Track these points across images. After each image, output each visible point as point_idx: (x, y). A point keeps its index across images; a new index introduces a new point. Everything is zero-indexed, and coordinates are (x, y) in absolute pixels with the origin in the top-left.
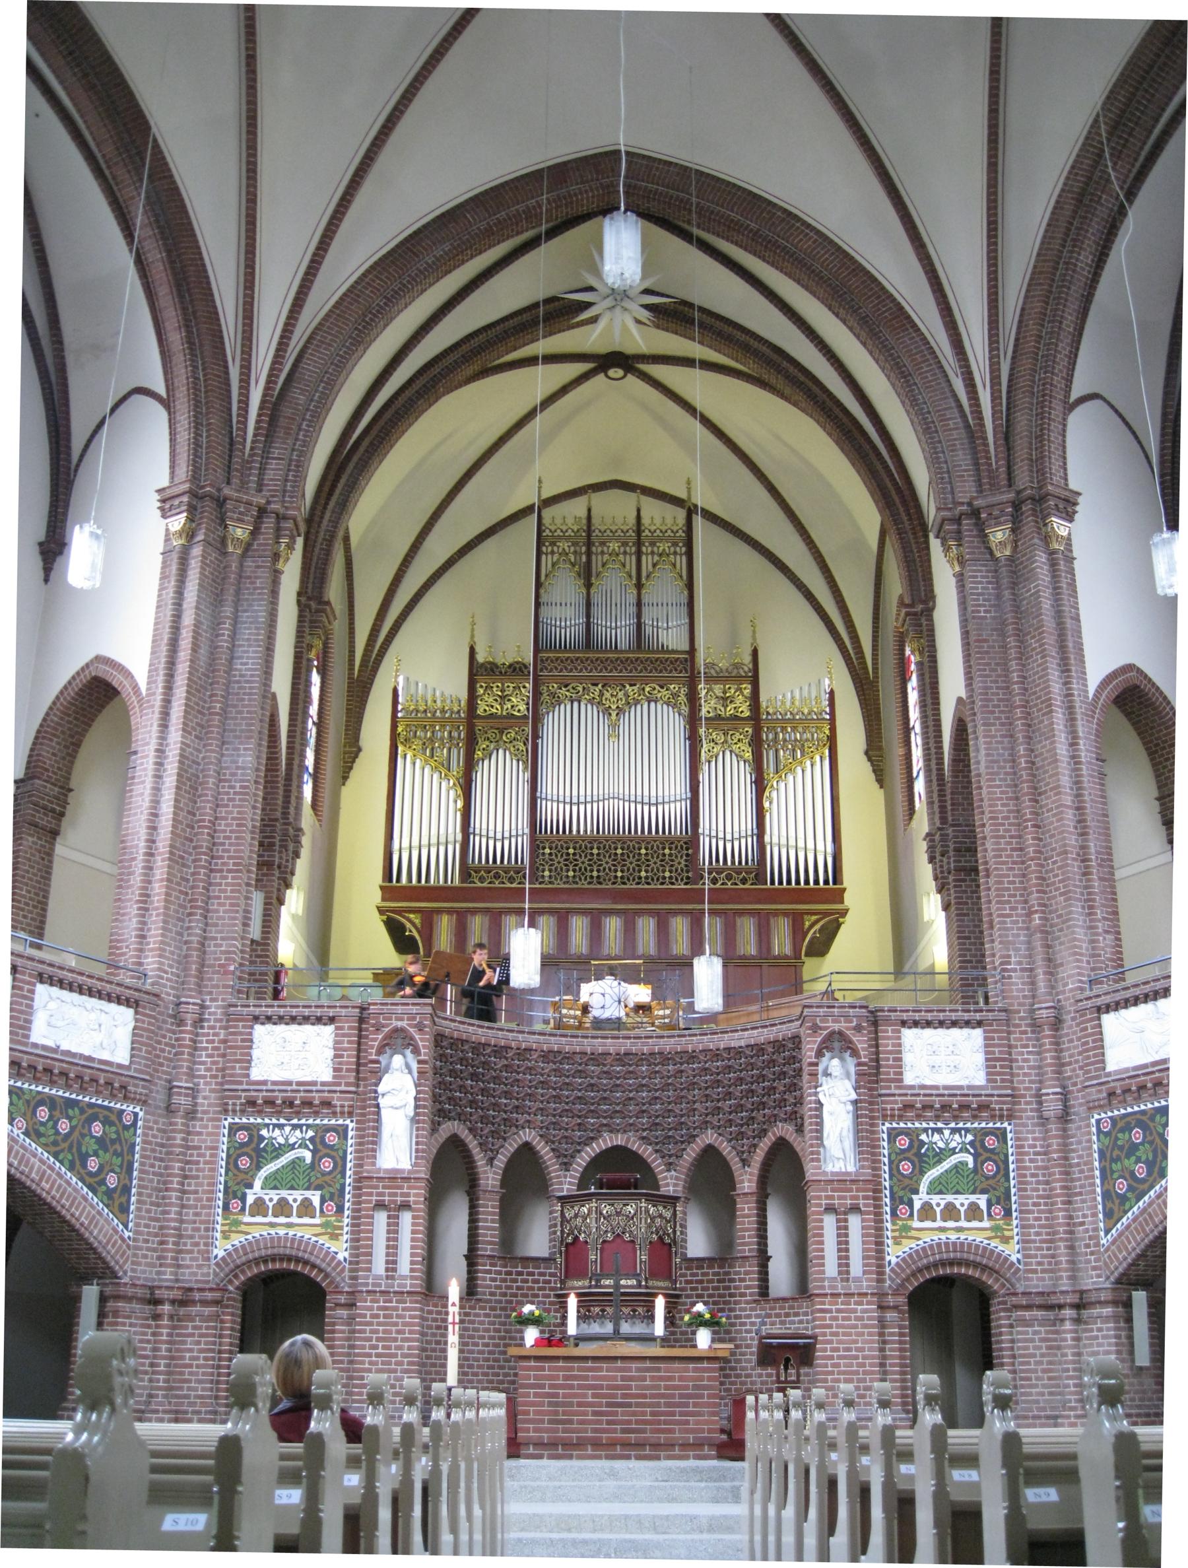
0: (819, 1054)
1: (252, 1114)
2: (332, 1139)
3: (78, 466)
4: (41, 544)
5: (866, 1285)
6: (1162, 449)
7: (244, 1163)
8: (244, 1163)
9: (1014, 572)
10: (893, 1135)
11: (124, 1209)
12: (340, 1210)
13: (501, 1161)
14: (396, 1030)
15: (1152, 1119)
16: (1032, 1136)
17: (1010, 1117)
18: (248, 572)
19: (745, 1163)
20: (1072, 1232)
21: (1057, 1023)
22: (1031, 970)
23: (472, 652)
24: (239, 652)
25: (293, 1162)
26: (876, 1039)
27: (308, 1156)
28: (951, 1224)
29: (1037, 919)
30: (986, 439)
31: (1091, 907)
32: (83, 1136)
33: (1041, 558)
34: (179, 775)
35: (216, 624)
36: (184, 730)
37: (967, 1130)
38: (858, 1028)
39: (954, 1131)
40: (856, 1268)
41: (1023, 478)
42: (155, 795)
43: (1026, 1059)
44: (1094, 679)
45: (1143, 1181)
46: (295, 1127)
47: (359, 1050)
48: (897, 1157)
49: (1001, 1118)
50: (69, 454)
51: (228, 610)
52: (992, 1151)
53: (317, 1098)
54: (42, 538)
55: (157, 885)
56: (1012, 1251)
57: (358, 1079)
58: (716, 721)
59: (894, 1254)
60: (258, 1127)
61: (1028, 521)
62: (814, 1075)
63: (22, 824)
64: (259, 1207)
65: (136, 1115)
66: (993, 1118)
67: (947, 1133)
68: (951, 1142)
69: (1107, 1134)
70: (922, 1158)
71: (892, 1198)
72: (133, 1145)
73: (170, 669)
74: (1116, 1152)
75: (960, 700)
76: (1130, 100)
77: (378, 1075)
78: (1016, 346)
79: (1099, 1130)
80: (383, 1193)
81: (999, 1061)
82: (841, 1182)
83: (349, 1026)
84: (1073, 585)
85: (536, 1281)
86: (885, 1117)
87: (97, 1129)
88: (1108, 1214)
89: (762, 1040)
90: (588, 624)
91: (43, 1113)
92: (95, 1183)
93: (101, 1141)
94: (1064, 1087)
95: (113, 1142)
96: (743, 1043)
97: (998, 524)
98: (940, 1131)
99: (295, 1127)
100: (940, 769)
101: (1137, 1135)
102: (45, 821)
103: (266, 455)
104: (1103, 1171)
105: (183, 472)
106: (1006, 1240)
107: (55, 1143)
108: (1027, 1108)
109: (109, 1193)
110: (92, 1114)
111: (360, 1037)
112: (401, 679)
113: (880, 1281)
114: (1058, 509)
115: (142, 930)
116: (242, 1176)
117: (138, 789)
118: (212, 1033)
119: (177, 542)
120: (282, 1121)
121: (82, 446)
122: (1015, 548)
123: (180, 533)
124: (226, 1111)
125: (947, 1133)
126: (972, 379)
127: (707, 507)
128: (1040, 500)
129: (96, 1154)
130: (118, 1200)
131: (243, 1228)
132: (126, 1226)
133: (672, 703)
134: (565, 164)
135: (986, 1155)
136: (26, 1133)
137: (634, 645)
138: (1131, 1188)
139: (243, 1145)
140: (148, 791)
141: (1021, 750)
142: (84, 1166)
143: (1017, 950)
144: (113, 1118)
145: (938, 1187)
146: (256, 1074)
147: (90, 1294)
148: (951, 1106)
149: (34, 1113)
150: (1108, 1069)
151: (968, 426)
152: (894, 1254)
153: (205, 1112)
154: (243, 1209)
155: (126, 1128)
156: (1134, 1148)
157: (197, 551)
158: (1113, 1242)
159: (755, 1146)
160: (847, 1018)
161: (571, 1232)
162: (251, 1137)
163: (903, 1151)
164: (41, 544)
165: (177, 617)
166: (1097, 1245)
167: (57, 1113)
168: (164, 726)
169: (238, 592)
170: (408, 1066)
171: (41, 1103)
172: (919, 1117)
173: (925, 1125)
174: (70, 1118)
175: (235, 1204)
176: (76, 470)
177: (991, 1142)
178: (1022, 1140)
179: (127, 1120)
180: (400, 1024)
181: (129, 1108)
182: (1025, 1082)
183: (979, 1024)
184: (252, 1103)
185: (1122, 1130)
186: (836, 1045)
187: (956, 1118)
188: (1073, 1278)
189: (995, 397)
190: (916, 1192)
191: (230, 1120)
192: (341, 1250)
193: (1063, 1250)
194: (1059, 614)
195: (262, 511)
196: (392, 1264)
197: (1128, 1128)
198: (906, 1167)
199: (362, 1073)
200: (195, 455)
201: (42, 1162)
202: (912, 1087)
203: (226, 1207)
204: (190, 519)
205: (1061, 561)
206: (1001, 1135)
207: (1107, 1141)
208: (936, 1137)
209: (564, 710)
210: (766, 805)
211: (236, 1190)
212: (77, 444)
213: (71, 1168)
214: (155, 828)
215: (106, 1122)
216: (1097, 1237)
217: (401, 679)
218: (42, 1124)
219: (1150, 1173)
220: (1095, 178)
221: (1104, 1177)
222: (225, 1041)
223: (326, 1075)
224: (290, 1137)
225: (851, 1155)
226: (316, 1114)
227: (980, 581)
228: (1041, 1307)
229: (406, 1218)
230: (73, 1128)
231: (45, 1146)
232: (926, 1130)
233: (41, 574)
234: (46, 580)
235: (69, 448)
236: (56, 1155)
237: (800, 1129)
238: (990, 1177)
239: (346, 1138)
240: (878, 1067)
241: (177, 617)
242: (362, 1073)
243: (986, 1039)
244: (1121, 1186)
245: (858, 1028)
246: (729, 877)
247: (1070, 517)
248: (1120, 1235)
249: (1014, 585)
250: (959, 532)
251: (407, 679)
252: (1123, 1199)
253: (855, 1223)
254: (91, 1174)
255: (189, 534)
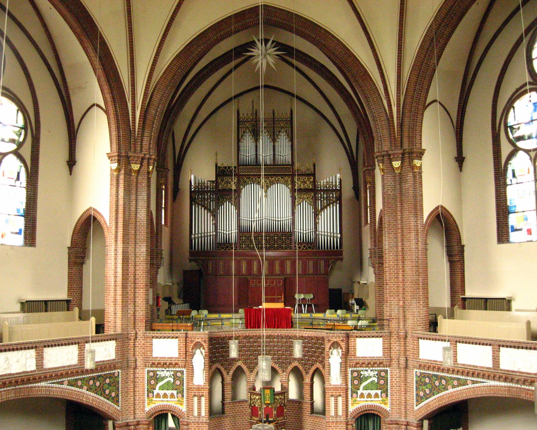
0: (330, 348)
1: (154, 367)
2: (179, 374)
3: (78, 129)
4: (67, 162)
5: (343, 419)
6: (457, 121)
7: (153, 382)
8: (153, 382)
9: (401, 178)
10: (352, 372)
11: (118, 401)
12: (183, 396)
13: (231, 373)
14: (197, 342)
15: (432, 377)
16: (396, 372)
17: (390, 366)
18: (140, 181)
19: (307, 373)
20: (406, 403)
21: (406, 337)
22: (399, 319)
23: (216, 165)
24: (139, 211)
25: (168, 382)
26: (348, 342)
27: (172, 380)
28: (369, 399)
29: (401, 303)
30: (394, 126)
31: (419, 300)
32: (103, 384)
33: (411, 175)
34: (123, 259)
35: (130, 201)
36: (123, 243)
37: (376, 370)
38: (343, 340)
39: (371, 370)
40: (340, 413)
41: (406, 146)
42: (115, 265)
43: (396, 347)
44: (427, 211)
45: (427, 394)
46: (167, 371)
47: (186, 347)
48: (353, 379)
49: (386, 366)
50: (74, 127)
51: (134, 197)
52: (383, 377)
53: (174, 363)
54: (68, 160)
55: (119, 287)
56: (388, 408)
57: (186, 356)
58: (300, 190)
59: (351, 409)
60: (156, 371)
61: (407, 160)
62: (328, 355)
63: (71, 264)
64: (158, 395)
65: (118, 372)
66: (384, 367)
67: (369, 371)
68: (370, 374)
69: (418, 377)
70: (360, 379)
71: (352, 392)
72: (119, 382)
73: (117, 220)
74: (421, 383)
75: (381, 210)
76: (452, 6)
77: (192, 356)
78: (406, 91)
79: (416, 375)
80: (196, 392)
81: (387, 349)
82: (336, 388)
83: (183, 340)
84: (421, 183)
85: (243, 408)
86: (350, 367)
87: (108, 381)
88: (417, 401)
89: (313, 335)
90: (256, 154)
91: (91, 382)
92: (108, 397)
93: (109, 384)
94: (406, 358)
95: (113, 383)
96: (307, 335)
97: (396, 161)
98: (367, 371)
99: (167, 371)
100: (375, 230)
101: (427, 380)
102: (79, 260)
103: (143, 136)
104: (416, 387)
105: (115, 146)
106: (386, 404)
107: (96, 390)
108: (394, 363)
109: (113, 398)
110: (105, 377)
111: (186, 342)
112: (192, 176)
113: (347, 416)
114: (417, 157)
115: (115, 297)
116: (152, 386)
117: (109, 261)
118: (140, 341)
119: (115, 174)
120: (163, 369)
121: (78, 122)
122: (401, 170)
123: (116, 170)
124: (146, 367)
125: (369, 371)
126: (390, 103)
127: (298, 95)
128: (411, 153)
129: (108, 388)
130: (116, 400)
131: (153, 402)
132: (118, 406)
133: (286, 183)
134: (244, 11)
135: (381, 378)
136: (87, 390)
137: (272, 163)
138: (424, 395)
139: (152, 377)
140: (113, 263)
141: (400, 244)
142: (105, 393)
143: (394, 312)
144: (112, 376)
145: (366, 388)
146: (154, 355)
147: (110, 423)
148: (371, 363)
149: (89, 383)
150: (420, 357)
151: (388, 119)
152: (351, 409)
153: (140, 367)
154: (153, 396)
155: (116, 377)
156: (425, 384)
157: (122, 177)
158: (418, 409)
159: (310, 369)
160: (339, 337)
161: (253, 403)
162: (154, 374)
163: (355, 377)
164: (67, 162)
165: (117, 201)
166: (413, 408)
167: (95, 381)
168: (116, 241)
169: (137, 191)
170: (202, 353)
171: (91, 379)
172: (361, 367)
173: (362, 369)
174: (99, 381)
175: (151, 394)
176: (77, 133)
177: (383, 374)
178: (393, 374)
179: (116, 375)
180: (198, 340)
181: (116, 371)
182: (394, 355)
183: (381, 337)
184: (153, 364)
185: (423, 377)
186: (335, 346)
187: (372, 367)
188: (406, 416)
189: (398, 111)
190: (359, 389)
191: (147, 369)
192: (184, 408)
193: (403, 408)
194: (415, 196)
195: (143, 159)
196: (199, 413)
197: (424, 377)
198: (356, 382)
199: (187, 355)
200: (118, 141)
201: (93, 396)
202: (359, 357)
203: (148, 396)
204: (119, 165)
205: (418, 175)
206: (386, 372)
207: (418, 379)
208: (366, 373)
209: (248, 187)
210: (317, 221)
211: (151, 390)
212: (76, 123)
213: (101, 396)
214: (116, 277)
215: (110, 378)
216: (413, 406)
217: (192, 176)
218: (92, 385)
219: (430, 393)
220: (438, 33)
221: (416, 390)
222: (144, 344)
223: (177, 355)
224: (166, 374)
225: (339, 379)
226: (174, 367)
227: (390, 181)
228: (395, 424)
229: (203, 399)
230: (100, 384)
231: (93, 392)
232: (363, 370)
233: (69, 172)
234: (71, 174)
235: (73, 125)
236: (96, 394)
237: (324, 367)
238: (382, 385)
239: (183, 374)
240: (348, 351)
241: (117, 201)
242: (187, 355)
243: (383, 342)
244: (421, 394)
245: (343, 340)
246: (304, 246)
247: (420, 158)
248: (420, 408)
249: (401, 183)
250: (383, 160)
251: (195, 178)
252: (422, 398)
253: (340, 399)
254: (107, 395)
255: (118, 170)
